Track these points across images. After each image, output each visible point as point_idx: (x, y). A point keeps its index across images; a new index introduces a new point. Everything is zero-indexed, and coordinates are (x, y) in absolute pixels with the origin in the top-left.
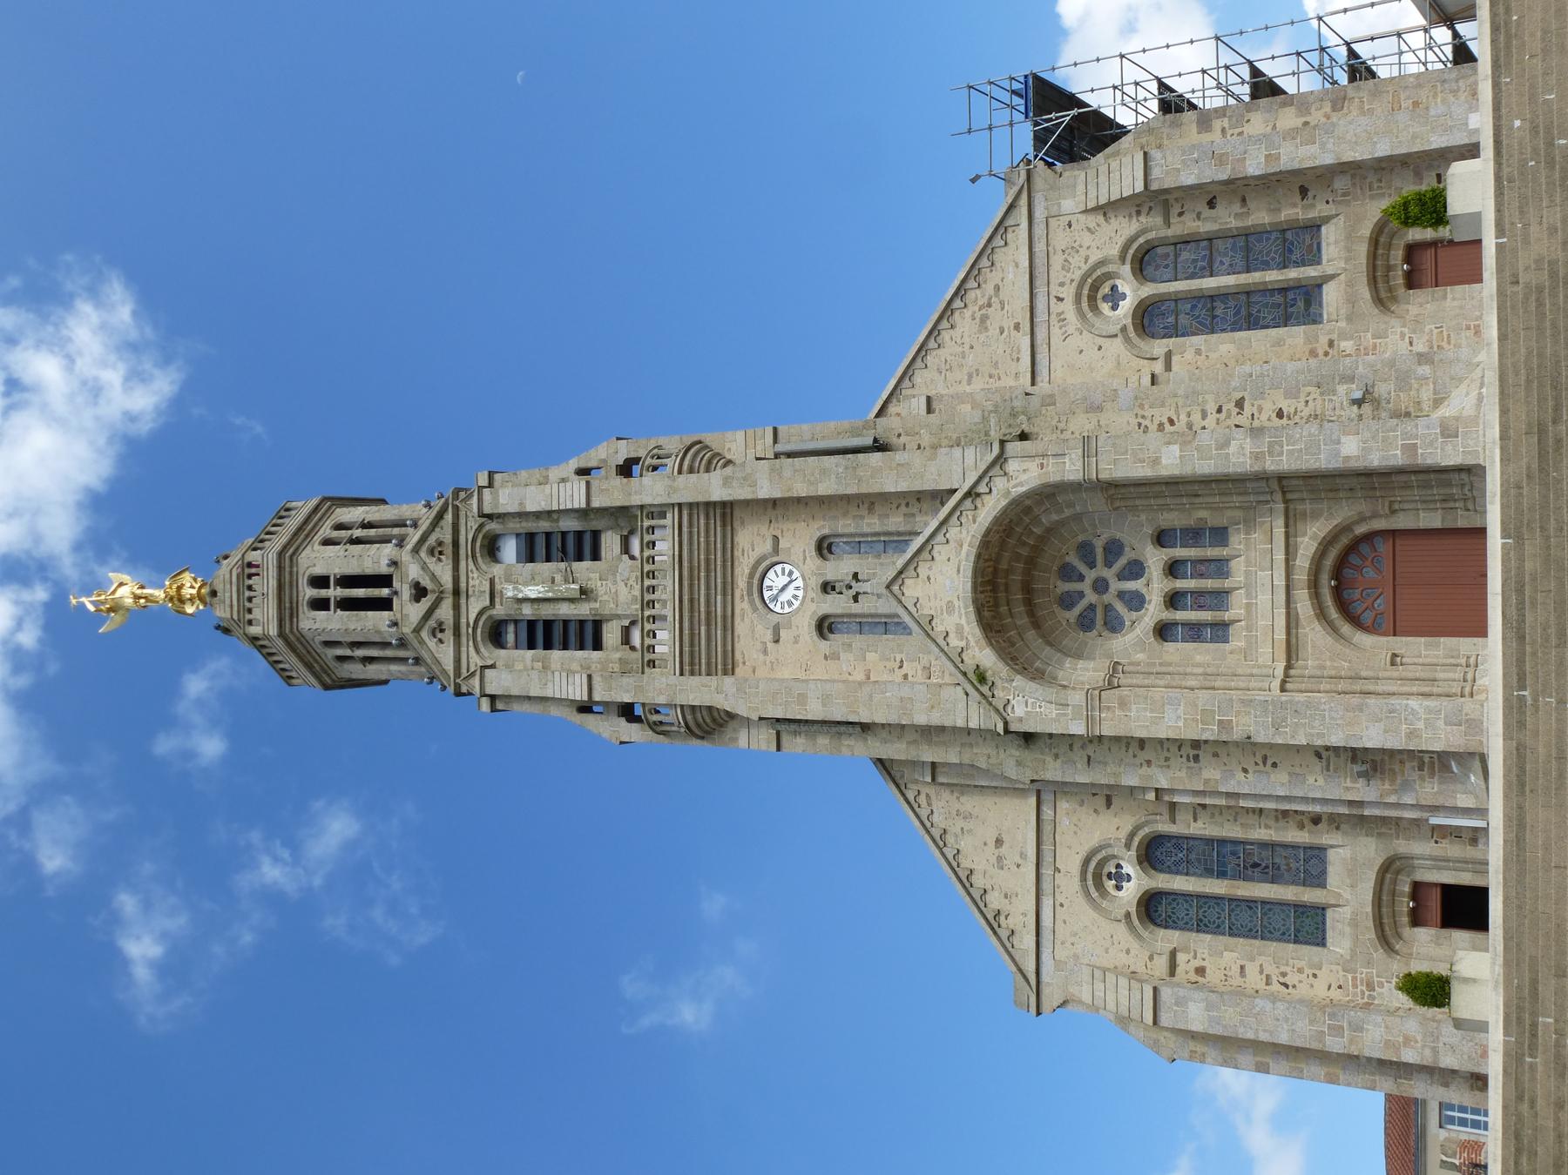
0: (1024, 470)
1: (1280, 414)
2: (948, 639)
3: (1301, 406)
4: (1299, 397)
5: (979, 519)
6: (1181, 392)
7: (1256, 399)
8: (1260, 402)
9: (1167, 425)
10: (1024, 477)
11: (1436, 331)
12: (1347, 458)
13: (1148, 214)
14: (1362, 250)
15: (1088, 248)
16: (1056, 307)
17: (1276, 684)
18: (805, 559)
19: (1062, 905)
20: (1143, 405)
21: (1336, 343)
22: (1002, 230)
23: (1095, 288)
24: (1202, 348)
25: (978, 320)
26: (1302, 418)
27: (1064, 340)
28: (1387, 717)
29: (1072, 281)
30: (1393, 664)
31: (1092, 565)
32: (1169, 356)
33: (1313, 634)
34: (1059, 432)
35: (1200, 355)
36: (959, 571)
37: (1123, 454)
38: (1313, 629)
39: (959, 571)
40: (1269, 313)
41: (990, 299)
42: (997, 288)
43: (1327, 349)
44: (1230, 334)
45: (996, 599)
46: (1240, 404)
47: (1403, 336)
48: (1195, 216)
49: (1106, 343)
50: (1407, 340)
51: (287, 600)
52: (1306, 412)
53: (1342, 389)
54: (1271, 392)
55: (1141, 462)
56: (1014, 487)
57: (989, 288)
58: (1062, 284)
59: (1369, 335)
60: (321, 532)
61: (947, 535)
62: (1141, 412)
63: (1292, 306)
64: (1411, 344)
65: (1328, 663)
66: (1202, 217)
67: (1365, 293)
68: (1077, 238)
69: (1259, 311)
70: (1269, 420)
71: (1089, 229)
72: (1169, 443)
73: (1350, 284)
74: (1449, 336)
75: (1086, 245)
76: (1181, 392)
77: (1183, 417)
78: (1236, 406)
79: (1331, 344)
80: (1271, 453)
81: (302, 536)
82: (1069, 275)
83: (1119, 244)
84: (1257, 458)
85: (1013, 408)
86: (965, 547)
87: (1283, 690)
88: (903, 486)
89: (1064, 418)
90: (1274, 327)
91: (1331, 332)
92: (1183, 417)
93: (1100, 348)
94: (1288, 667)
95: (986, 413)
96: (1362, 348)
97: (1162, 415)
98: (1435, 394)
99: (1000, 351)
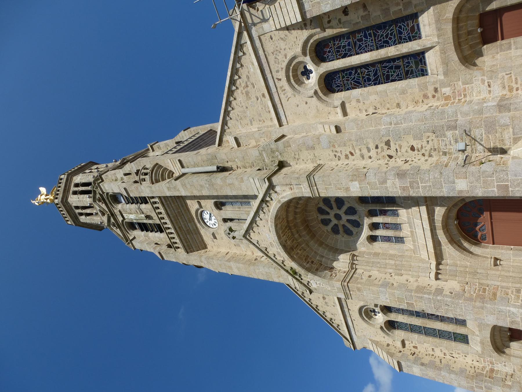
0: (283, 190)
1: (413, 149)
2: (276, 257)
3: (425, 144)
4: (422, 139)
5: (271, 211)
6: (353, 138)
7: (397, 141)
8: (400, 142)
9: (350, 156)
10: (285, 194)
11: (506, 77)
12: (461, 191)
13: (311, 25)
14: (449, 28)
15: (285, 49)
16: (279, 84)
17: (433, 275)
18: (212, 210)
19: (354, 320)
20: (335, 146)
21: (439, 89)
22: (239, 47)
23: (295, 70)
24: (360, 98)
25: (245, 94)
26: (426, 151)
27: (288, 101)
28: (498, 314)
29: (282, 69)
30: (496, 265)
31: (328, 213)
32: (343, 105)
33: (448, 249)
34: (297, 160)
35: (360, 102)
36: (270, 231)
37: (329, 185)
38: (448, 248)
39: (270, 231)
40: (394, 72)
41: (246, 83)
42: (248, 77)
43: (434, 93)
44: (373, 87)
45: (292, 232)
46: (388, 143)
47: (483, 81)
48: (337, 22)
49: (309, 100)
50: (486, 84)
51: (72, 214)
52: (428, 147)
53: (449, 134)
54: (405, 136)
55: (340, 189)
56: (282, 198)
57: (244, 77)
58: (278, 71)
59: (460, 83)
60: (71, 189)
61: (260, 217)
62: (334, 149)
63: (407, 66)
64: (489, 86)
65: (458, 262)
66: (342, 21)
67: (454, 56)
68: (277, 45)
69: (388, 72)
70: (406, 152)
71: (282, 39)
72: (352, 181)
73: (443, 52)
74: (516, 79)
75: (283, 48)
76: (353, 138)
77: (357, 151)
78: (386, 144)
79: (436, 90)
80: (412, 187)
81: (66, 192)
82: (279, 66)
83: (300, 45)
84: (404, 190)
85: (271, 149)
86: (269, 223)
87: (437, 278)
88: (234, 193)
89: (297, 153)
90: (399, 80)
91: (434, 83)
92: (357, 151)
93: (306, 103)
94: (438, 264)
95: (260, 151)
96: (456, 91)
97: (347, 150)
98: (514, 134)
99: (260, 108)
